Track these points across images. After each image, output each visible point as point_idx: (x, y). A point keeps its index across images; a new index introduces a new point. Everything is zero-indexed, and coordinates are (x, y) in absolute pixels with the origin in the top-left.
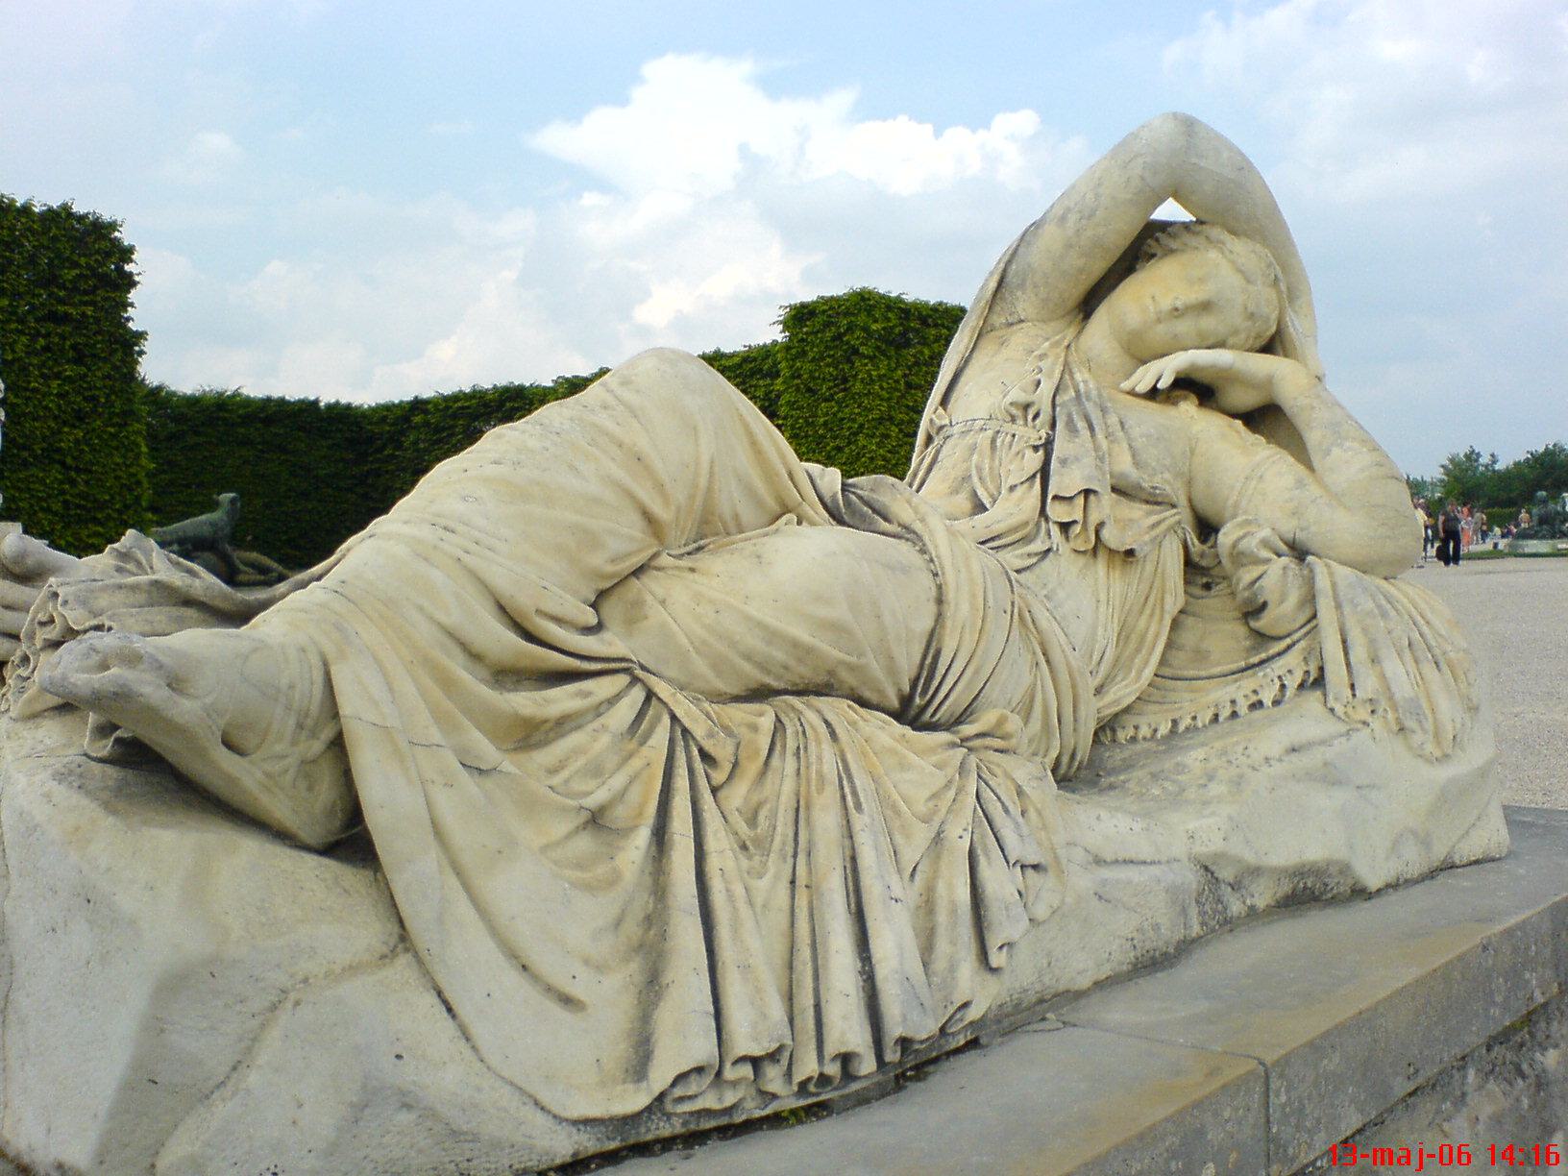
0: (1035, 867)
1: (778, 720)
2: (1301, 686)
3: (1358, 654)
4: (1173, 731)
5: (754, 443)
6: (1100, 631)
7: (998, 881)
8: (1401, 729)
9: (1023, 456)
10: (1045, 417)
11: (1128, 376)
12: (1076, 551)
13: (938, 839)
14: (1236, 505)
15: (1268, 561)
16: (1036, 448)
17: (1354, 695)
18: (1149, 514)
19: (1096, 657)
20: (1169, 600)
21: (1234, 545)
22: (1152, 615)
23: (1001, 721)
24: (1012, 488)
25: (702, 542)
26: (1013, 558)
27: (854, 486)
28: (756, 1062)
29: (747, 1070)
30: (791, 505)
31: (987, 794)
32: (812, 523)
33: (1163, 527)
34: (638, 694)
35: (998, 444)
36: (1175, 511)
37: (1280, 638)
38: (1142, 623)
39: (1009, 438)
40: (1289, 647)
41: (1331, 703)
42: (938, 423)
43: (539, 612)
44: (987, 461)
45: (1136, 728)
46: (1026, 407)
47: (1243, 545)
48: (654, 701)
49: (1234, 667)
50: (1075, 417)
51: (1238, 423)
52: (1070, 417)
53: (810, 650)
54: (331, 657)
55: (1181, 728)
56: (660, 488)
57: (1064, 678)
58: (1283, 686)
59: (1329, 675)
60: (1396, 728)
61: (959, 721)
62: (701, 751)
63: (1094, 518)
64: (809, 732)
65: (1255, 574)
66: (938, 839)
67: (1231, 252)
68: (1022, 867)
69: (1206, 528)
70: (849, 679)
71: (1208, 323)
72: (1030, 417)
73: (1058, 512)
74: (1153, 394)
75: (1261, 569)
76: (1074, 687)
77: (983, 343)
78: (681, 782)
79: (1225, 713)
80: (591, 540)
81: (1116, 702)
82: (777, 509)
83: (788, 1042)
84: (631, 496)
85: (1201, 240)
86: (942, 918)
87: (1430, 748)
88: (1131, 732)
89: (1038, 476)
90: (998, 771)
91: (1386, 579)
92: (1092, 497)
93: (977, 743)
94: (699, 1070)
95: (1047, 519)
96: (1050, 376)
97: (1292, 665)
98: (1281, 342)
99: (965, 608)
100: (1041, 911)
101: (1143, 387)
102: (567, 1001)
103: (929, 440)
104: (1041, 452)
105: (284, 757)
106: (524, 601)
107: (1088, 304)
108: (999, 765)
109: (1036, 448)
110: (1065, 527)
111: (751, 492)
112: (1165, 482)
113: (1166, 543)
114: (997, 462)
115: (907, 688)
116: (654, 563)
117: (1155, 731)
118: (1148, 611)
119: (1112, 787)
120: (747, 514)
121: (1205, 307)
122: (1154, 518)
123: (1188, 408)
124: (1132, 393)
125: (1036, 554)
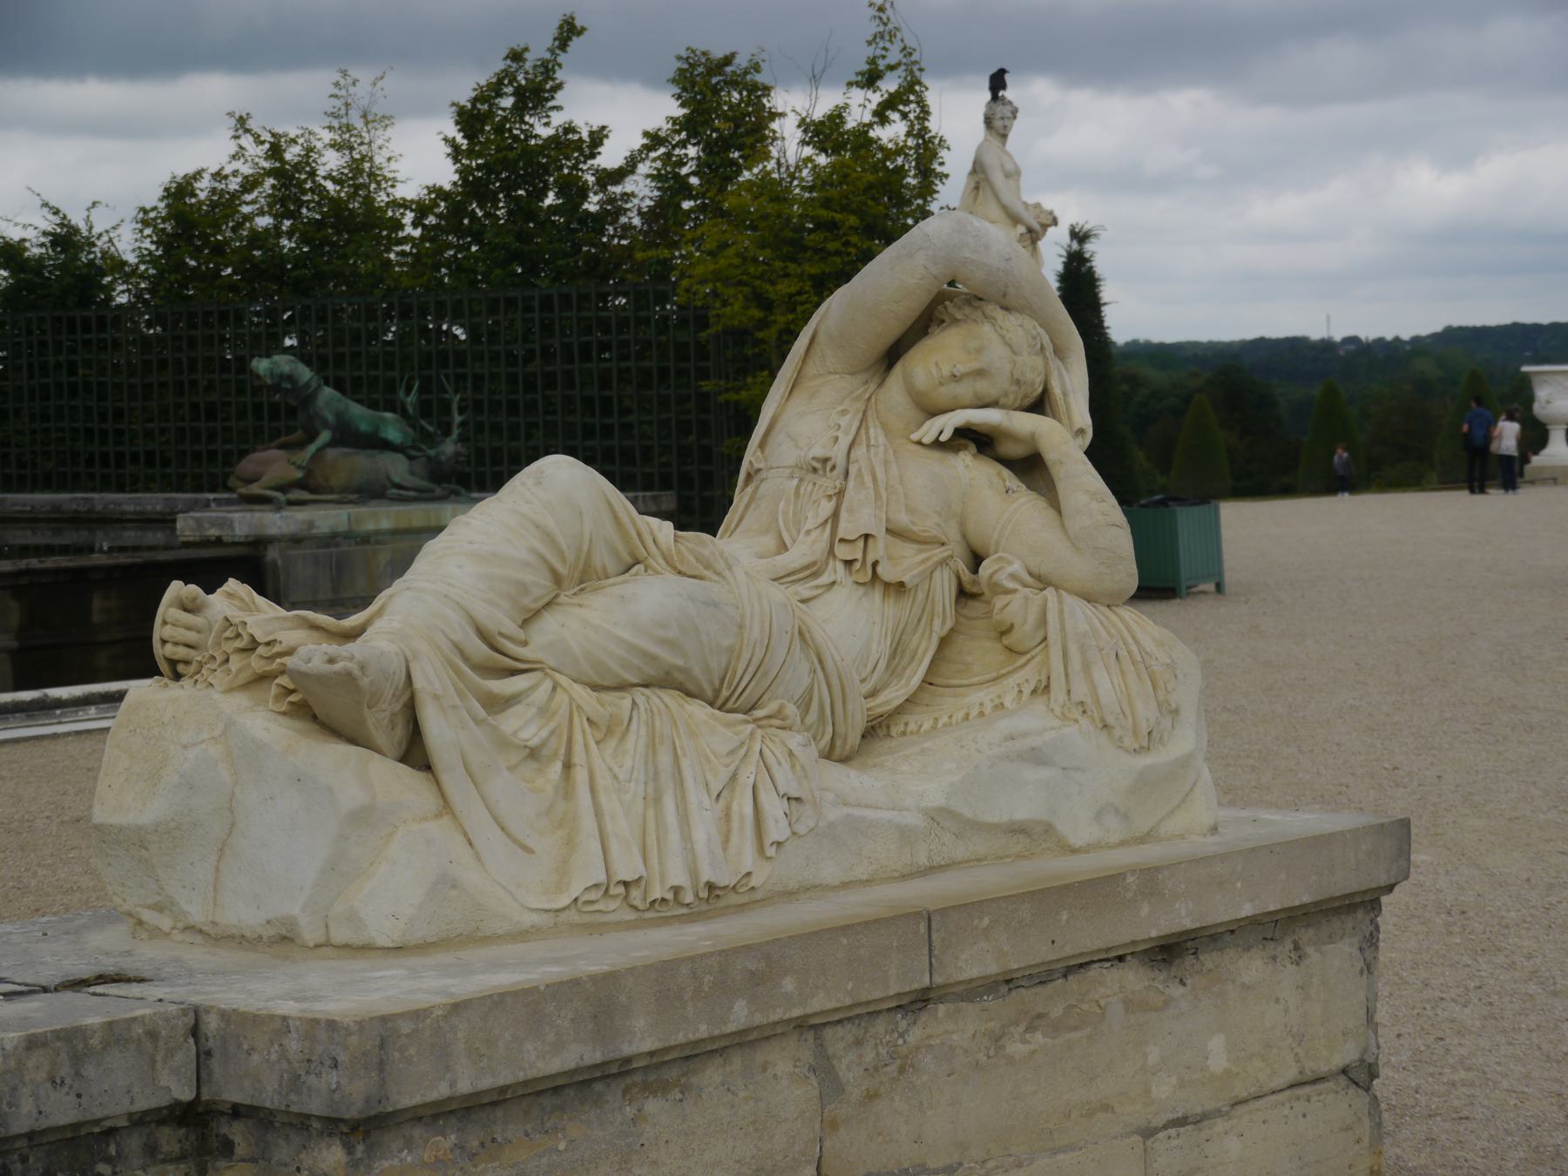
0: (798, 799)
1: (634, 703)
2: (1034, 692)
3: (1076, 663)
4: (934, 728)
5: (616, 517)
6: (874, 646)
7: (773, 807)
8: (1105, 726)
9: (819, 504)
10: (839, 470)
11: (920, 425)
12: (857, 583)
13: (734, 778)
14: (997, 543)
15: (1014, 591)
16: (830, 497)
17: (1069, 699)
18: (920, 551)
19: (870, 667)
20: (937, 622)
21: (991, 576)
22: (923, 634)
23: (781, 709)
24: (808, 532)
25: (583, 586)
26: (805, 590)
27: (680, 537)
28: (626, 884)
29: (621, 890)
30: (640, 559)
31: (767, 752)
32: (657, 573)
33: (930, 563)
34: (548, 685)
35: (802, 492)
36: (943, 548)
37: (1027, 653)
38: (916, 639)
39: (810, 486)
40: (1029, 660)
41: (1052, 705)
42: (757, 466)
43: (501, 634)
44: (792, 507)
45: (906, 724)
46: (825, 460)
47: (996, 578)
48: (559, 689)
49: (988, 677)
50: (864, 470)
51: (1006, 473)
52: (860, 470)
53: (653, 658)
54: (409, 659)
55: (940, 725)
56: (560, 553)
57: (835, 681)
58: (1021, 691)
59: (1053, 684)
60: (1100, 725)
61: (753, 707)
62: (588, 719)
63: (870, 560)
64: (655, 710)
65: (1005, 602)
66: (734, 778)
67: (1001, 328)
68: (788, 799)
69: (976, 560)
70: (680, 677)
71: (985, 388)
72: (828, 469)
73: (843, 552)
74: (937, 444)
75: (1009, 597)
76: (843, 689)
77: (796, 393)
78: (578, 737)
79: (975, 712)
80: (523, 588)
81: (887, 702)
82: (629, 560)
83: (644, 874)
84: (545, 561)
85: (979, 314)
86: (735, 824)
87: (1128, 742)
88: (902, 729)
89: (830, 521)
90: (777, 740)
91: (1108, 606)
92: (871, 541)
93: (764, 722)
94: (596, 886)
95: (835, 557)
96: (847, 433)
97: (1028, 676)
98: (1050, 404)
99: (756, 630)
100: (801, 829)
101: (927, 440)
102: (525, 848)
103: (749, 477)
104: (834, 499)
105: (384, 711)
106: (491, 626)
107: (892, 355)
108: (776, 736)
109: (830, 497)
110: (849, 563)
111: (614, 552)
112: (928, 525)
113: (937, 574)
114: (799, 508)
115: (717, 683)
116: (557, 601)
117: (920, 727)
118: (920, 631)
119: (875, 766)
120: (612, 567)
121: (980, 373)
122: (924, 556)
123: (968, 467)
124: (919, 443)
125: (822, 586)
